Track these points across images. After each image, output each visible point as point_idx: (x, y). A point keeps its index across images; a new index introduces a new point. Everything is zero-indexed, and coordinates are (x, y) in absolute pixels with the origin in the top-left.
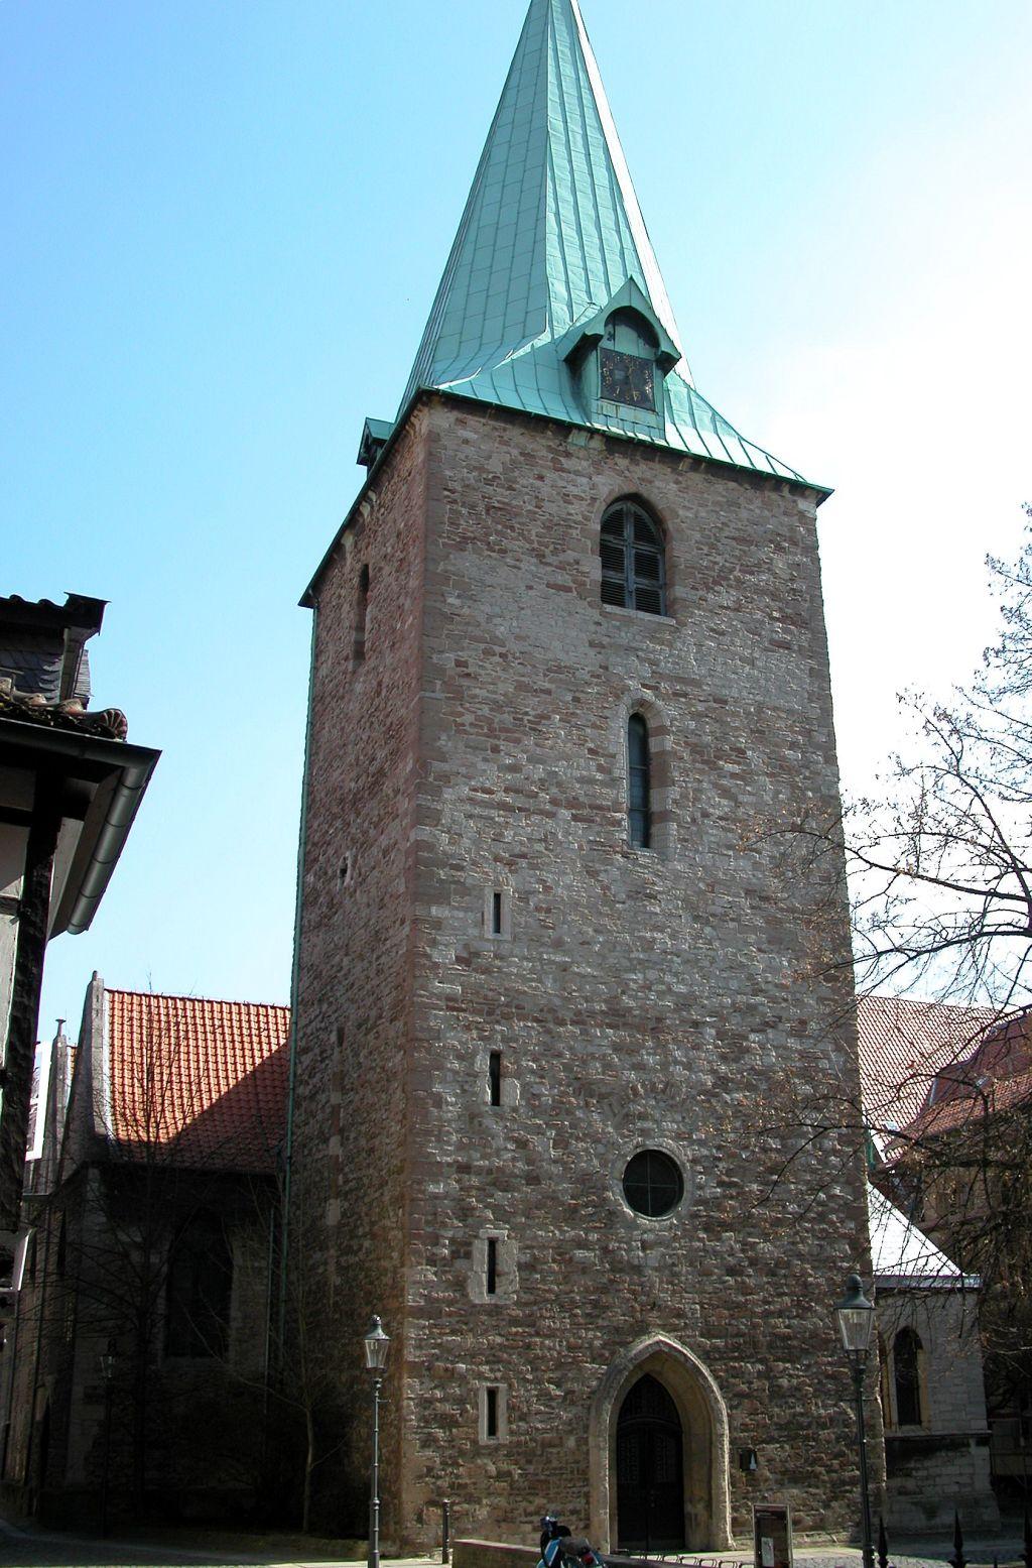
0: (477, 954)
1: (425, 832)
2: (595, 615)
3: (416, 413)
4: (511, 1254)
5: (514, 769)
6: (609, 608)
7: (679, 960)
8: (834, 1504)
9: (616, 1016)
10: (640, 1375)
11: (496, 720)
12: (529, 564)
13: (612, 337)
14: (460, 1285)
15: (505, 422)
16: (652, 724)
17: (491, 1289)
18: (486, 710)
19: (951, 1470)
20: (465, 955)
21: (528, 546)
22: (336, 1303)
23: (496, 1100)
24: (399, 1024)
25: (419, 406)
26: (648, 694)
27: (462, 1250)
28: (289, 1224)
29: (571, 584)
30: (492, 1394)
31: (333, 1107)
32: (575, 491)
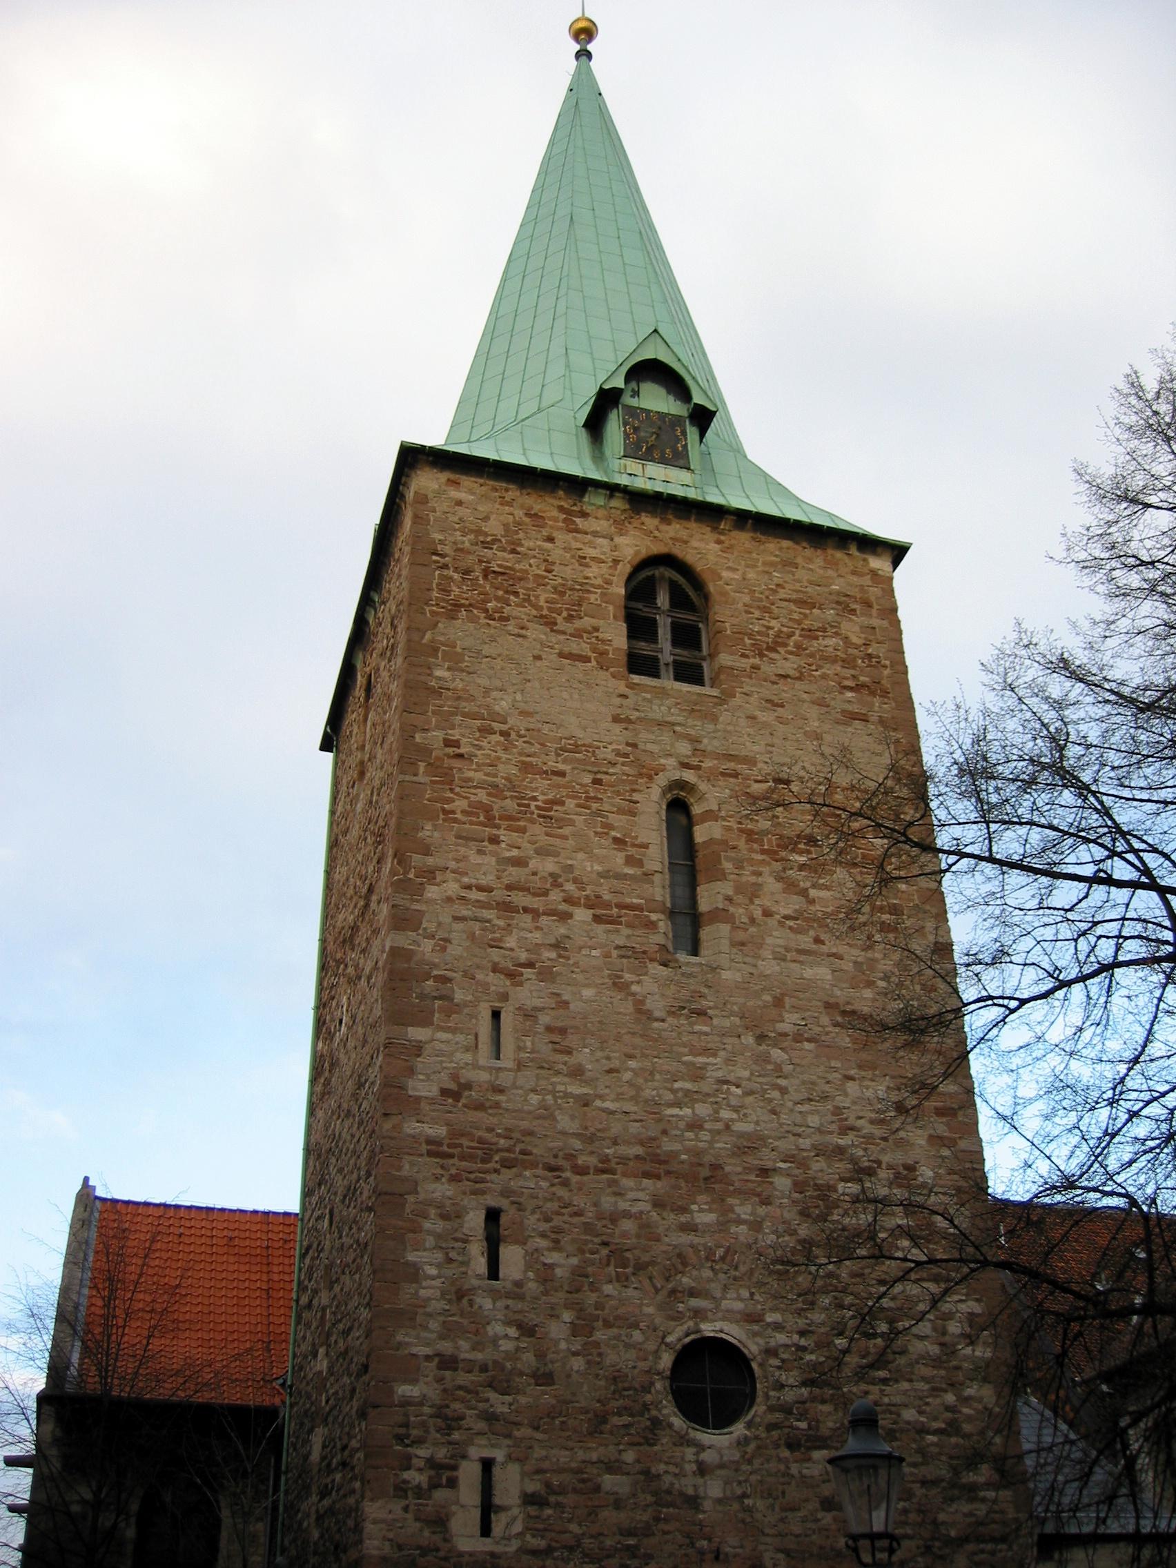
0: (468, 1086)
3: (404, 479)
5: (519, 862)
6: (636, 678)
12: (536, 632)
14: (440, 1522)
16: (697, 810)
17: (486, 1530)
18: (482, 796)
23: (494, 1273)
26: (689, 776)
27: (443, 1473)
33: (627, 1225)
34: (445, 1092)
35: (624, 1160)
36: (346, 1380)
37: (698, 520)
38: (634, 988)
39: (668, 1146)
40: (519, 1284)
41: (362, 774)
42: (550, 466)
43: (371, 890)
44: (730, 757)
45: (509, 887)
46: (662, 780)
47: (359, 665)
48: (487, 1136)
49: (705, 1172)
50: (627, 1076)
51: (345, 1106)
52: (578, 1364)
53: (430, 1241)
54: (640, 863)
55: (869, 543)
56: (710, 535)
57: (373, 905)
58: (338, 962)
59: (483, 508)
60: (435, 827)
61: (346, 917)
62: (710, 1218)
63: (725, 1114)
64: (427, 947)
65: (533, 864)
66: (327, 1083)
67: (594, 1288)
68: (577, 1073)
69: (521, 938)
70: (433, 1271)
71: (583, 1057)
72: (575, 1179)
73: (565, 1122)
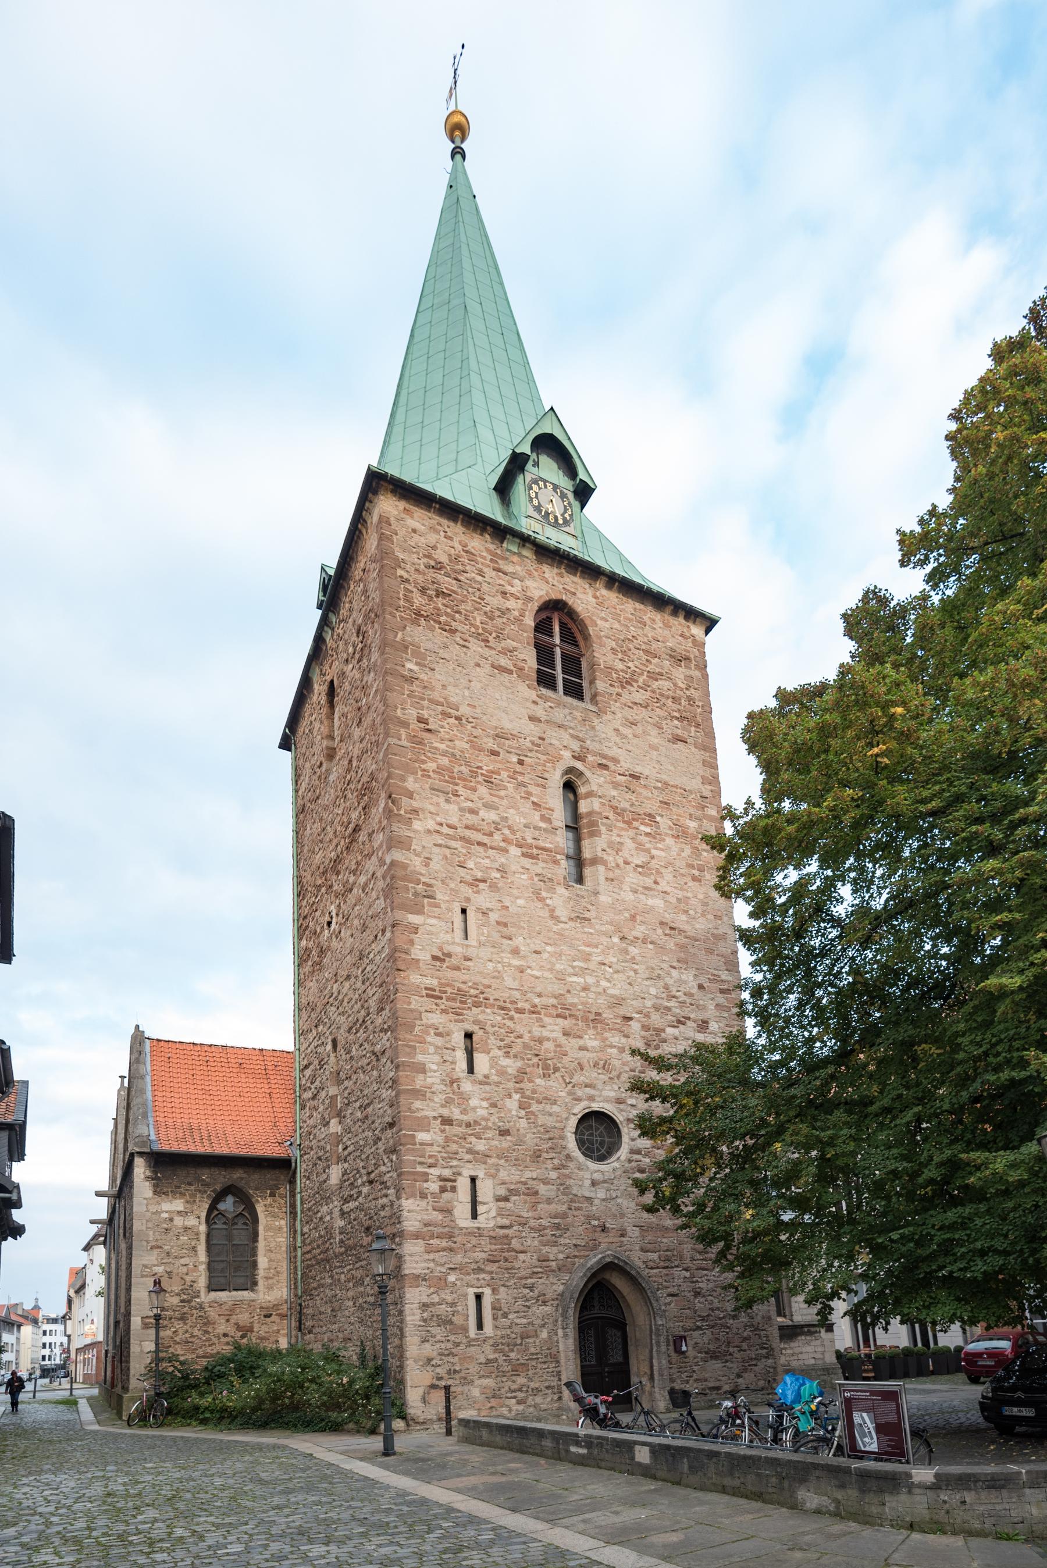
0: (449, 955)
1: (397, 855)
2: (533, 695)
4: (486, 1190)
5: (472, 811)
6: (544, 691)
7: (611, 970)
8: (1027, 389)
9: (564, 1012)
10: (594, 1282)
11: (455, 770)
12: (475, 646)
13: (536, 464)
14: (448, 1211)
15: (449, 519)
16: (582, 790)
17: (474, 1215)
18: (445, 761)
20: (440, 954)
21: (473, 630)
22: (342, 1241)
23: (471, 1070)
24: (386, 1013)
25: (370, 495)
26: (579, 765)
27: (448, 1185)
28: (301, 1192)
29: (512, 668)
30: (478, 1297)
31: (331, 1097)
32: (512, 590)
33: (549, 1045)
34: (435, 958)
35: (546, 1007)
38: (548, 901)
39: (571, 999)
40: (486, 1077)
44: (604, 757)
45: (467, 827)
46: (561, 767)
48: (463, 987)
49: (592, 1016)
50: (545, 956)
52: (523, 1124)
53: (432, 1050)
55: (691, 614)
56: (590, 591)
59: (432, 538)
64: (417, 863)
67: (530, 1081)
68: (516, 952)
69: (478, 862)
70: (434, 1067)
71: (519, 941)
72: (516, 1016)
73: (509, 982)
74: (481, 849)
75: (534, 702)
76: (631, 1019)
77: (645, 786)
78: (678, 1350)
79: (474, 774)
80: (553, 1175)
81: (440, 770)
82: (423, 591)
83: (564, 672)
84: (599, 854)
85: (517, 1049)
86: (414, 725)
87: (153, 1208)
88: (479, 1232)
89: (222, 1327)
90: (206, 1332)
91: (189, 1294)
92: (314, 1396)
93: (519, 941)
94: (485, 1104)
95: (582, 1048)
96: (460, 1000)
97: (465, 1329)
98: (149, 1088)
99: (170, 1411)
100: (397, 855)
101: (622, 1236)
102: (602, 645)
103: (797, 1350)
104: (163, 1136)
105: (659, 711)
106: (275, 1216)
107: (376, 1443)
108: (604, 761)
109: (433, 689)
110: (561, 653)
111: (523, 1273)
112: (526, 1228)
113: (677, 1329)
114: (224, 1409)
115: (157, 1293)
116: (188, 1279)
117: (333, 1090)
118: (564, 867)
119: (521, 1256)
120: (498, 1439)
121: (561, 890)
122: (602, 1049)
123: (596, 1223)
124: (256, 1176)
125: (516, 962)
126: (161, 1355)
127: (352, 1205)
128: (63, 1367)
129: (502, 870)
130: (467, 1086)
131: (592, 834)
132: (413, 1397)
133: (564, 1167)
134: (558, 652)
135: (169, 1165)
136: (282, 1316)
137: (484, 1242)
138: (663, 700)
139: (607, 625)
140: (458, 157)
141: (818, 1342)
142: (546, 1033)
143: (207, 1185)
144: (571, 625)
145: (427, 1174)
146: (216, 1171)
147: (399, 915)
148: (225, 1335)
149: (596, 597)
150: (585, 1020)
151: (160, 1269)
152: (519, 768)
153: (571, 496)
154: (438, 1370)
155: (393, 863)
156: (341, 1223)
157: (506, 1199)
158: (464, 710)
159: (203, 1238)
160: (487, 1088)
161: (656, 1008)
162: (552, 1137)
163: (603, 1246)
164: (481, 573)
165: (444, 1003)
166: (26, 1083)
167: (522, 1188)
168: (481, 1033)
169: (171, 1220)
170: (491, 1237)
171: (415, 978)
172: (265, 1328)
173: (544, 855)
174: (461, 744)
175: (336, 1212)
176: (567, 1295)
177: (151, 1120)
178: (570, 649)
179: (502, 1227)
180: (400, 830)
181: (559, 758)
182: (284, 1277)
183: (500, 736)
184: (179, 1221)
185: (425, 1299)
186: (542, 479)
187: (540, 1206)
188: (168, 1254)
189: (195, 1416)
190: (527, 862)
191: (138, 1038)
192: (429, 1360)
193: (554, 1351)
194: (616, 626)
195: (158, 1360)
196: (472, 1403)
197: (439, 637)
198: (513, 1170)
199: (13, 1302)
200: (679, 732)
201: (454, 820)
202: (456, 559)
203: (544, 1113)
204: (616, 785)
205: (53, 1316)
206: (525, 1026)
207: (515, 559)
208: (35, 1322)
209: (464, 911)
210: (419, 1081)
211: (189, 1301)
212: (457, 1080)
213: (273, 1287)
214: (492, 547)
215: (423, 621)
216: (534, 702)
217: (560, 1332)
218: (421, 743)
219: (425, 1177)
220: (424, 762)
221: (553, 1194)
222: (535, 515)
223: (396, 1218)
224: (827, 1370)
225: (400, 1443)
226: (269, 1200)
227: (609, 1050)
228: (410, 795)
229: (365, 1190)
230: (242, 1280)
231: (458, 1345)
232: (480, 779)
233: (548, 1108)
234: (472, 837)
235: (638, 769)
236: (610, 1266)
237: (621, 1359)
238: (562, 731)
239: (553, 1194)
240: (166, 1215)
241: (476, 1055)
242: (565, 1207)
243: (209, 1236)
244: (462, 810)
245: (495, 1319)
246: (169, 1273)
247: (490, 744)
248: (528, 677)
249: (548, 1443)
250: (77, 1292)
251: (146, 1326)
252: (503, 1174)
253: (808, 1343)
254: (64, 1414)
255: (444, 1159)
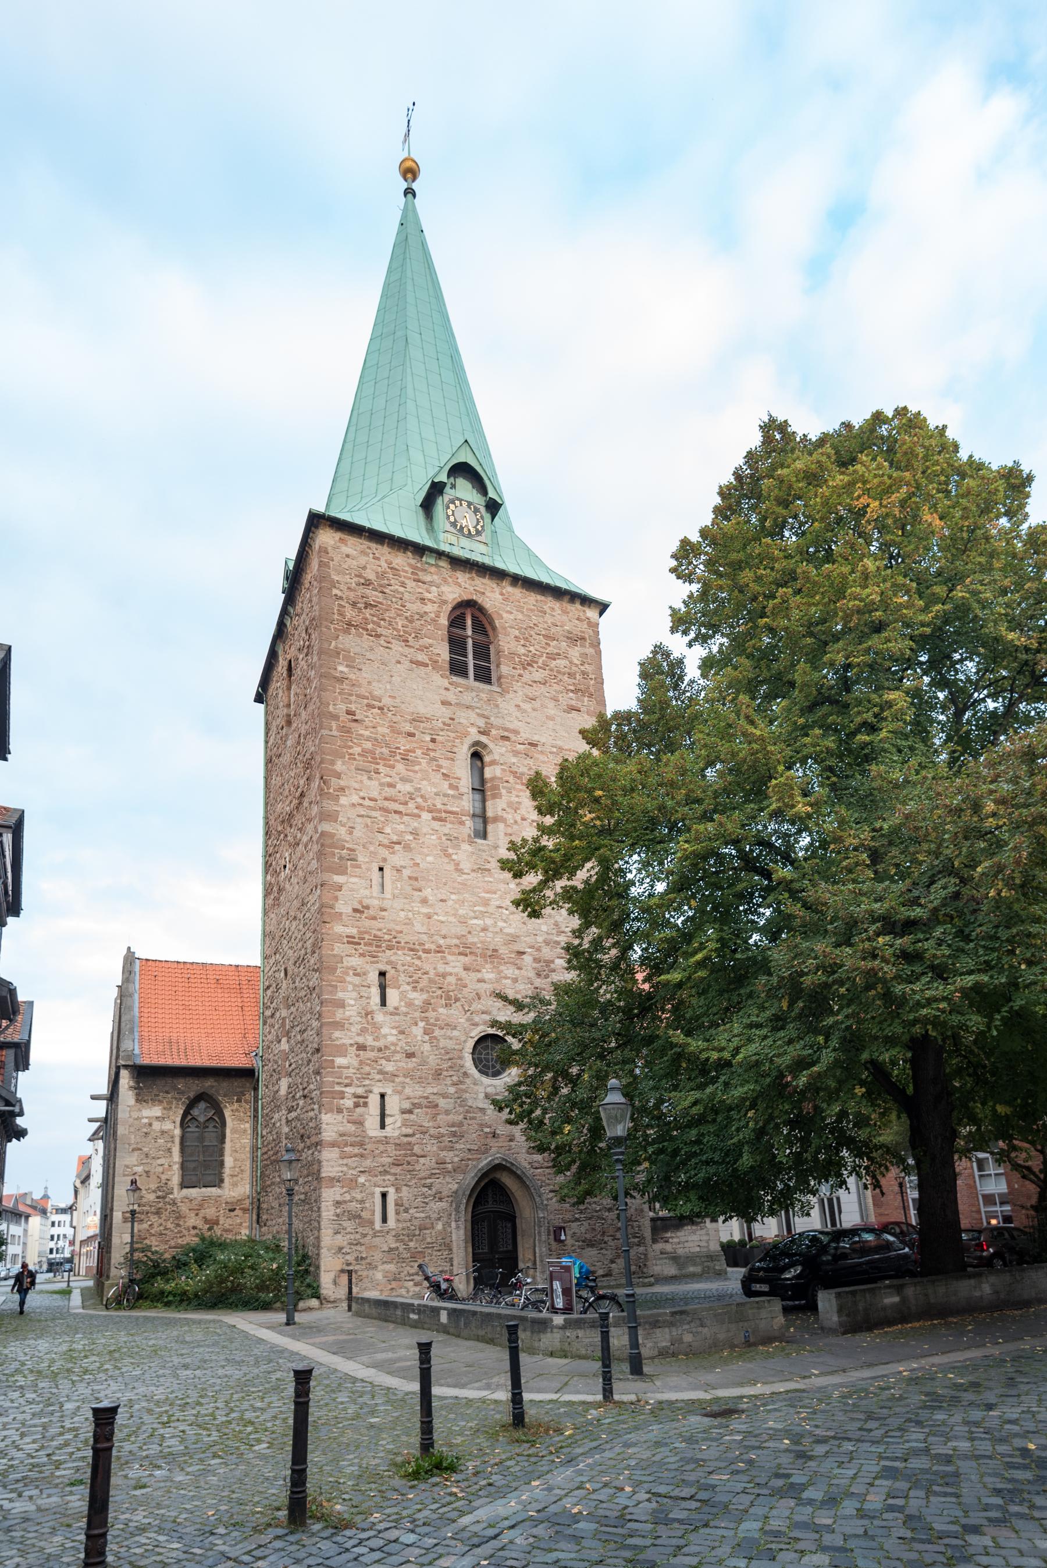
0: (367, 907)
1: (325, 827)
2: (445, 683)
4: (393, 1105)
5: (391, 785)
6: (455, 679)
9: (465, 950)
12: (397, 646)
13: (453, 486)
14: (360, 1123)
16: (487, 759)
17: (383, 1126)
18: (368, 745)
19: (695, 1238)
20: (360, 907)
23: (383, 1003)
26: (484, 739)
27: (361, 1101)
30: (384, 1195)
33: (451, 979)
34: (355, 910)
35: (449, 947)
36: (304, 1055)
37: (490, 579)
38: (454, 857)
39: (471, 939)
40: (396, 1008)
41: (289, 723)
42: (403, 536)
43: (302, 795)
44: (506, 730)
45: (386, 799)
46: (468, 741)
47: (280, 652)
48: (379, 933)
49: (489, 953)
50: (450, 903)
51: (292, 913)
52: (427, 1047)
53: (350, 988)
54: (456, 788)
55: (586, 601)
56: (497, 590)
57: (305, 804)
58: (280, 833)
59: (363, 560)
60: (344, 763)
61: (284, 807)
62: (492, 976)
63: (501, 924)
64: (342, 832)
65: (399, 786)
66: (276, 899)
67: (434, 1010)
68: (424, 901)
69: (394, 828)
70: (352, 1002)
71: (427, 892)
72: (424, 955)
73: (418, 927)
74: (397, 816)
75: (447, 689)
76: (524, 953)
77: (542, 752)
78: (558, 1240)
79: (393, 754)
80: (452, 1090)
81: (364, 753)
82: (354, 604)
83: (474, 658)
84: (500, 813)
85: (423, 983)
86: (344, 717)
87: (135, 1115)
88: (386, 1140)
89: (192, 1221)
90: (178, 1225)
91: (163, 1192)
92: (249, 1280)
93: (427, 892)
94: (394, 1032)
95: (480, 981)
96: (373, 944)
97: (372, 1223)
98: (137, 1005)
99: (140, 1296)
100: (325, 827)
101: (511, 1140)
102: (507, 635)
103: (683, 1239)
104: (145, 1051)
105: (556, 687)
106: (241, 1120)
107: (282, 1317)
108: (506, 734)
109: (360, 686)
110: (471, 644)
111: (423, 1174)
112: (427, 1136)
113: (558, 1223)
114: (185, 1293)
115: (134, 1191)
116: (164, 1177)
117: (284, 1013)
118: (470, 824)
119: (422, 1160)
120: (374, 1312)
121: (466, 846)
122: (498, 980)
123: (487, 1130)
124: (225, 1084)
125: (425, 910)
126: (136, 1246)
127: (293, 1115)
128: (70, 1261)
129: (415, 833)
130: (379, 1017)
131: (495, 796)
132: (326, 1280)
133: (461, 1082)
134: (470, 642)
135: (150, 1077)
136: (244, 1210)
137: (391, 1148)
138: (560, 677)
139: (512, 617)
140: (410, 196)
141: (703, 1232)
142: (449, 969)
143: (182, 1093)
144: (482, 618)
145: (343, 1092)
146: (190, 1081)
147: (326, 876)
148: (194, 1228)
149: (502, 594)
150: (483, 956)
151: (139, 1169)
152: (431, 746)
153: (483, 510)
154: (348, 1257)
155: (323, 834)
156: (286, 1129)
157: (410, 1112)
158: (386, 701)
159: (177, 1140)
160: (397, 1018)
161: (547, 943)
162: (452, 1057)
163: (493, 1150)
164: (403, 585)
165: (362, 948)
166: (31, 1003)
167: (424, 1102)
168: (393, 971)
169: (150, 1125)
170: (396, 1144)
171: (339, 929)
172: (229, 1221)
173: (451, 817)
174: (383, 730)
175: (284, 1121)
176: (460, 1192)
177: (136, 1034)
178: (481, 638)
179: (406, 1136)
180: (329, 805)
181: (466, 734)
182: (247, 1175)
183: (416, 720)
184: (157, 1126)
185: (338, 1198)
186: (458, 499)
187: (439, 1117)
188: (147, 1155)
189: (162, 1299)
190: (436, 825)
191: (130, 958)
192: (340, 1249)
193: (447, 1241)
194: (520, 616)
195: (133, 1250)
196: (376, 1285)
197: (367, 641)
198: (417, 1087)
199: (22, 1191)
200: (573, 703)
201: (375, 794)
202: (381, 576)
203: (445, 1037)
204: (516, 753)
205: (63, 1205)
206: (431, 964)
207: (433, 569)
208: (44, 1212)
209: (381, 869)
210: (339, 1015)
211: (164, 1197)
212: (372, 1012)
213: (237, 1183)
214: (413, 562)
215: (353, 630)
216: (447, 689)
217: (453, 1224)
218: (349, 731)
219: (342, 1095)
220: (351, 747)
221: (451, 1106)
222: (452, 529)
223: (318, 1130)
224: (711, 1257)
225: (298, 1317)
226: (236, 1105)
227: (504, 981)
228: (338, 776)
229: (301, 1102)
230: (210, 1178)
231: (365, 1236)
232: (398, 757)
233: (449, 1033)
234: (390, 807)
235: (536, 738)
236: (498, 1167)
237: (510, 1248)
238: (470, 711)
239: (451, 1106)
240: (146, 1121)
241: (388, 990)
242: (461, 1117)
243: (183, 1139)
244: (382, 784)
245: (397, 1213)
246: (147, 1172)
247: (408, 728)
248: (441, 668)
249: (399, 1312)
250: (83, 1182)
251: (125, 1220)
252: (408, 1091)
253: (694, 1232)
254: (58, 1301)
255: (358, 1079)
